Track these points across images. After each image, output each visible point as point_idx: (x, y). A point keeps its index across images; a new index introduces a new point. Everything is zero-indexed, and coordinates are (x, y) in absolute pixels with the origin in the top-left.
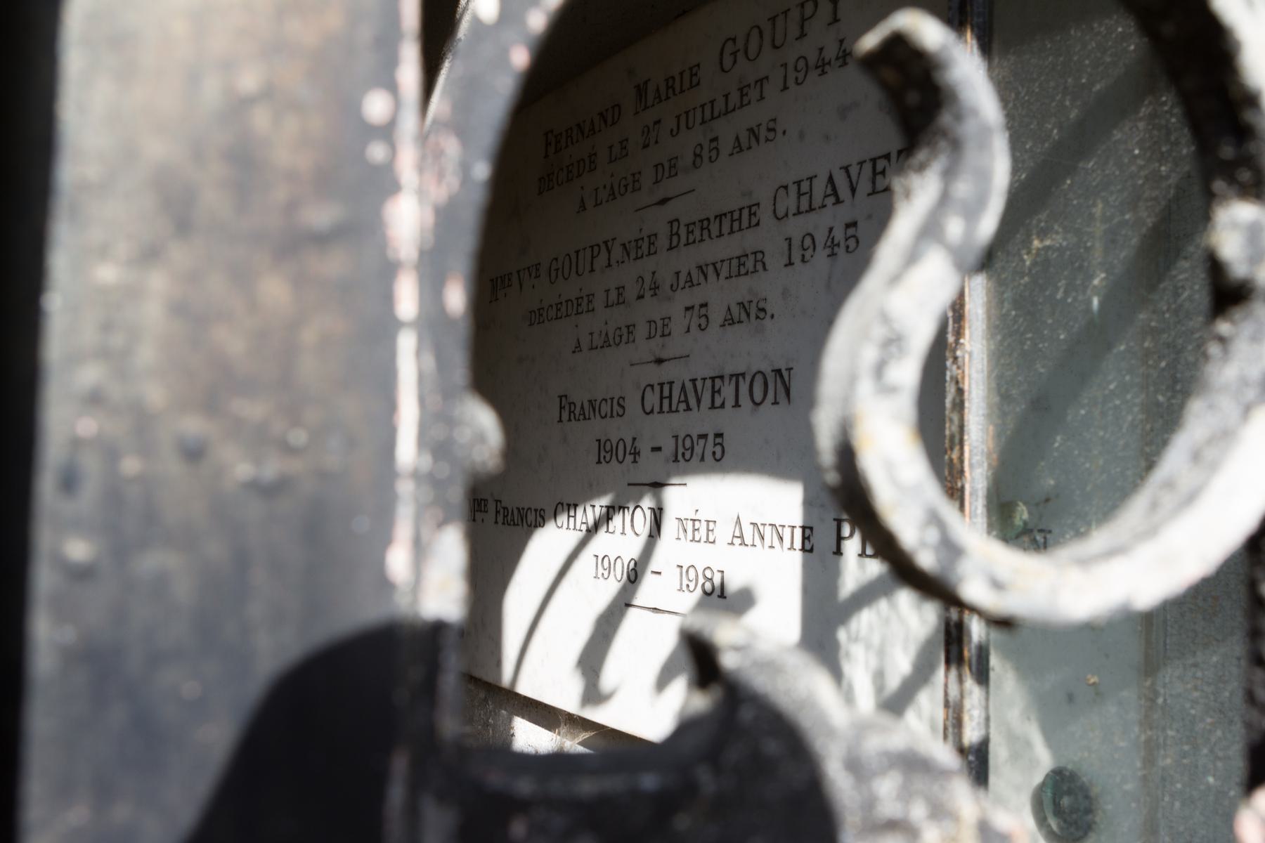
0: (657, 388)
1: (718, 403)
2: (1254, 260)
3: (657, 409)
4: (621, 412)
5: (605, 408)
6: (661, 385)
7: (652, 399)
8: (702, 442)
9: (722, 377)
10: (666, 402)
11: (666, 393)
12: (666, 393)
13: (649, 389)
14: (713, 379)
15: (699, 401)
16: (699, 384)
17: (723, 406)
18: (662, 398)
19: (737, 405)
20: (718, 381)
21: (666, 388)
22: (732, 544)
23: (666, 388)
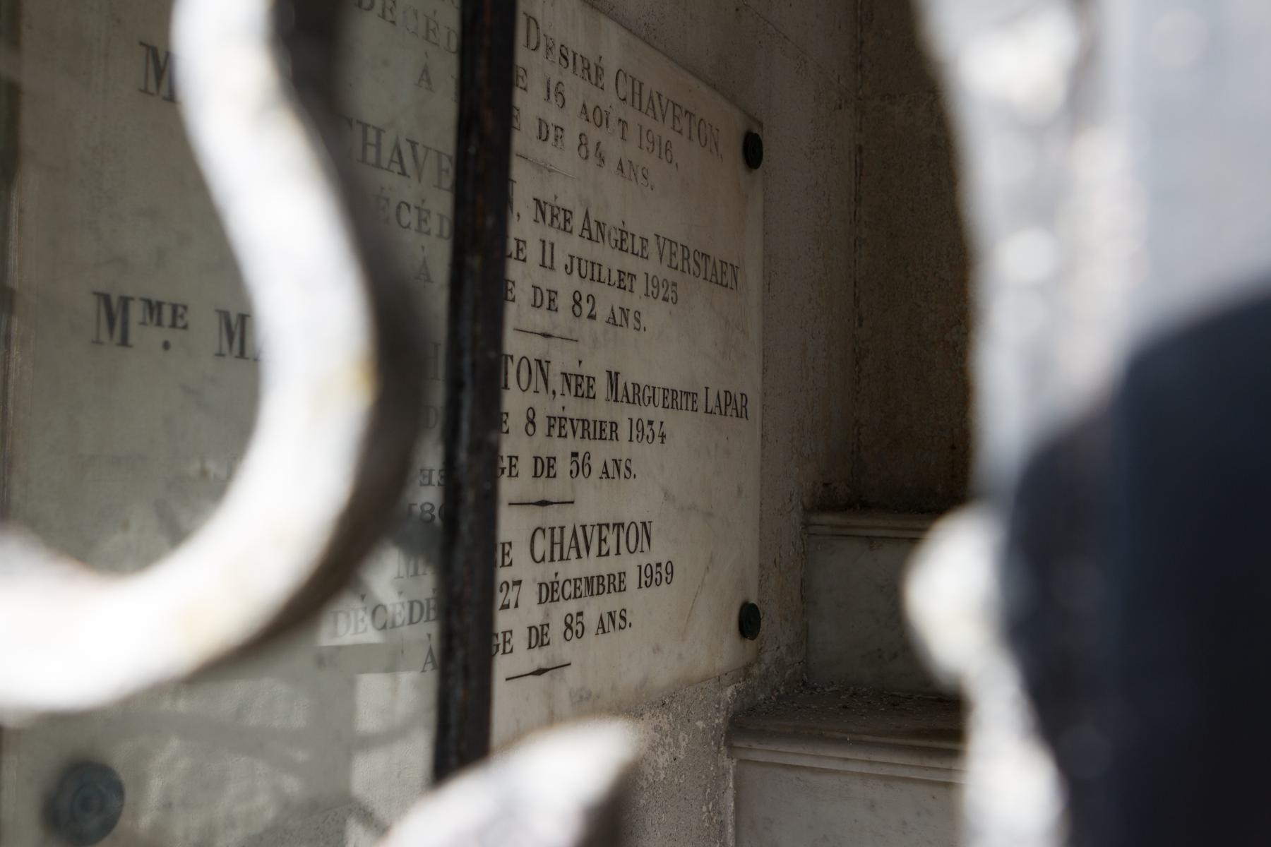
0: (548, 533)
1: (604, 552)
2: (323, 660)
3: (548, 557)
4: (623, 624)
5: (569, 589)
6: (553, 529)
7: (542, 545)
8: (516, 588)
9: (608, 526)
10: (557, 548)
11: (557, 539)
12: (557, 539)
13: (539, 533)
14: (600, 526)
15: (651, 98)
16: (589, 530)
17: (608, 554)
18: (553, 544)
19: (618, 553)
20: (604, 528)
21: (557, 532)
22: (524, 260)
23: (557, 532)
